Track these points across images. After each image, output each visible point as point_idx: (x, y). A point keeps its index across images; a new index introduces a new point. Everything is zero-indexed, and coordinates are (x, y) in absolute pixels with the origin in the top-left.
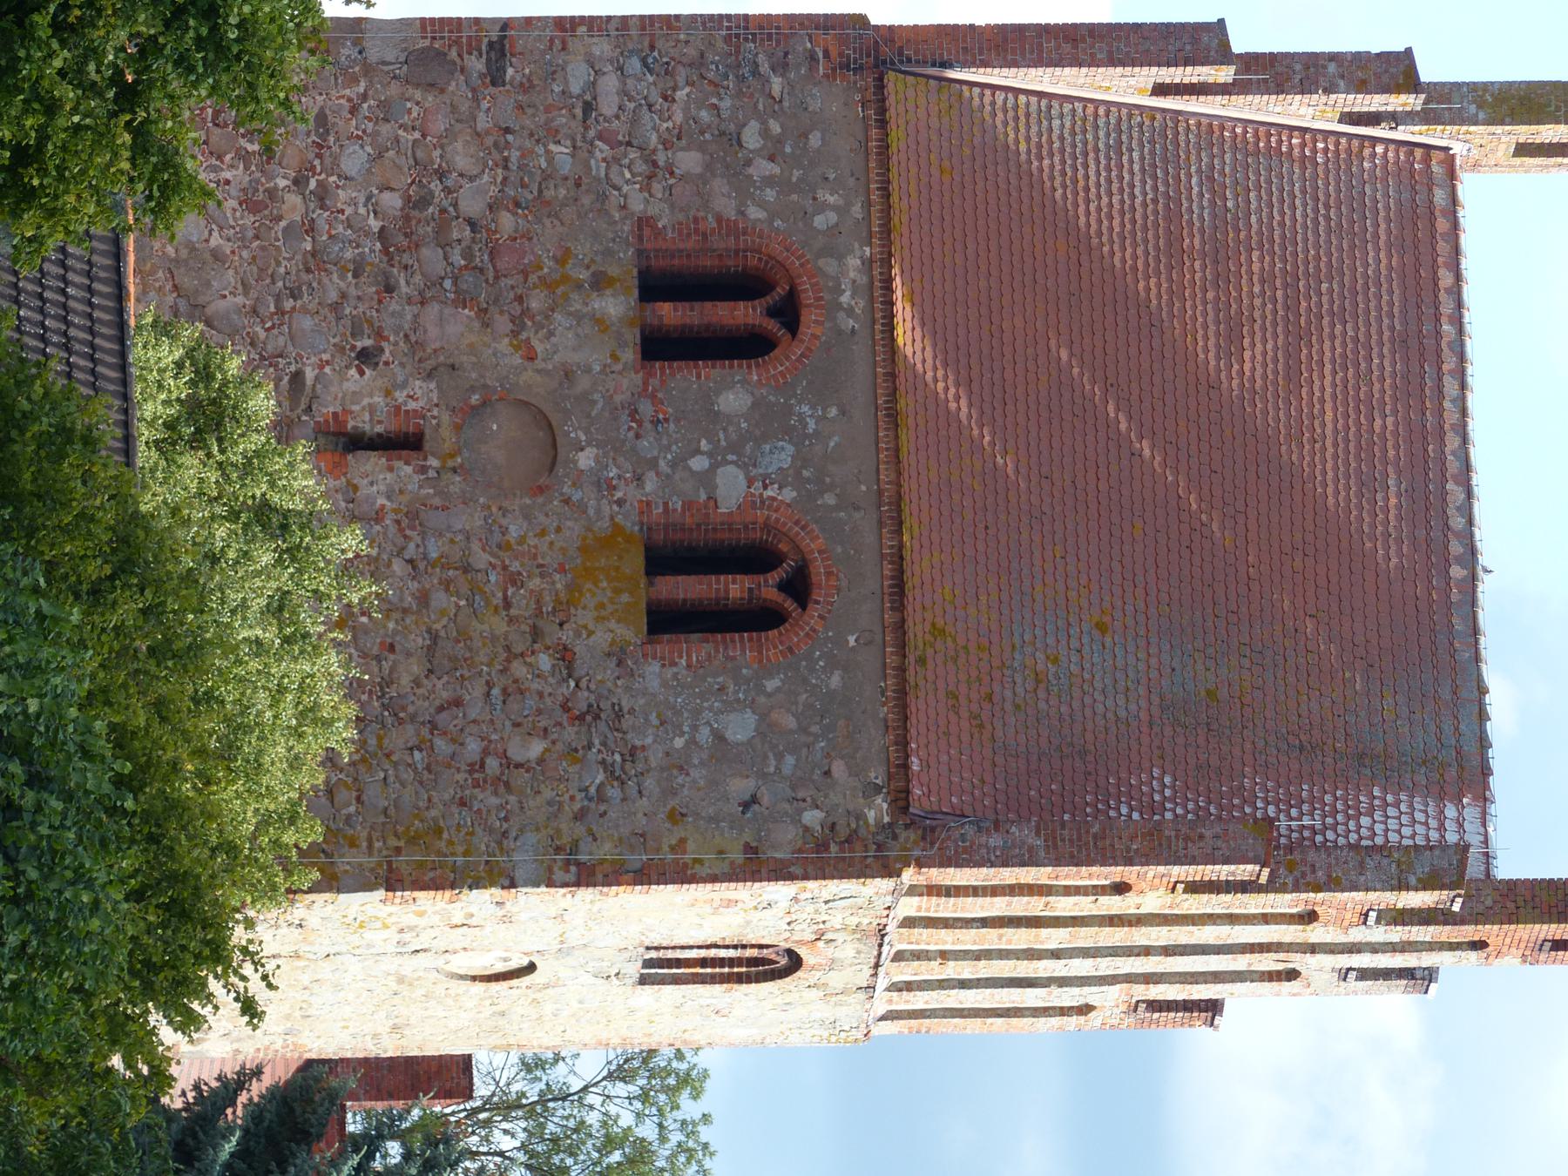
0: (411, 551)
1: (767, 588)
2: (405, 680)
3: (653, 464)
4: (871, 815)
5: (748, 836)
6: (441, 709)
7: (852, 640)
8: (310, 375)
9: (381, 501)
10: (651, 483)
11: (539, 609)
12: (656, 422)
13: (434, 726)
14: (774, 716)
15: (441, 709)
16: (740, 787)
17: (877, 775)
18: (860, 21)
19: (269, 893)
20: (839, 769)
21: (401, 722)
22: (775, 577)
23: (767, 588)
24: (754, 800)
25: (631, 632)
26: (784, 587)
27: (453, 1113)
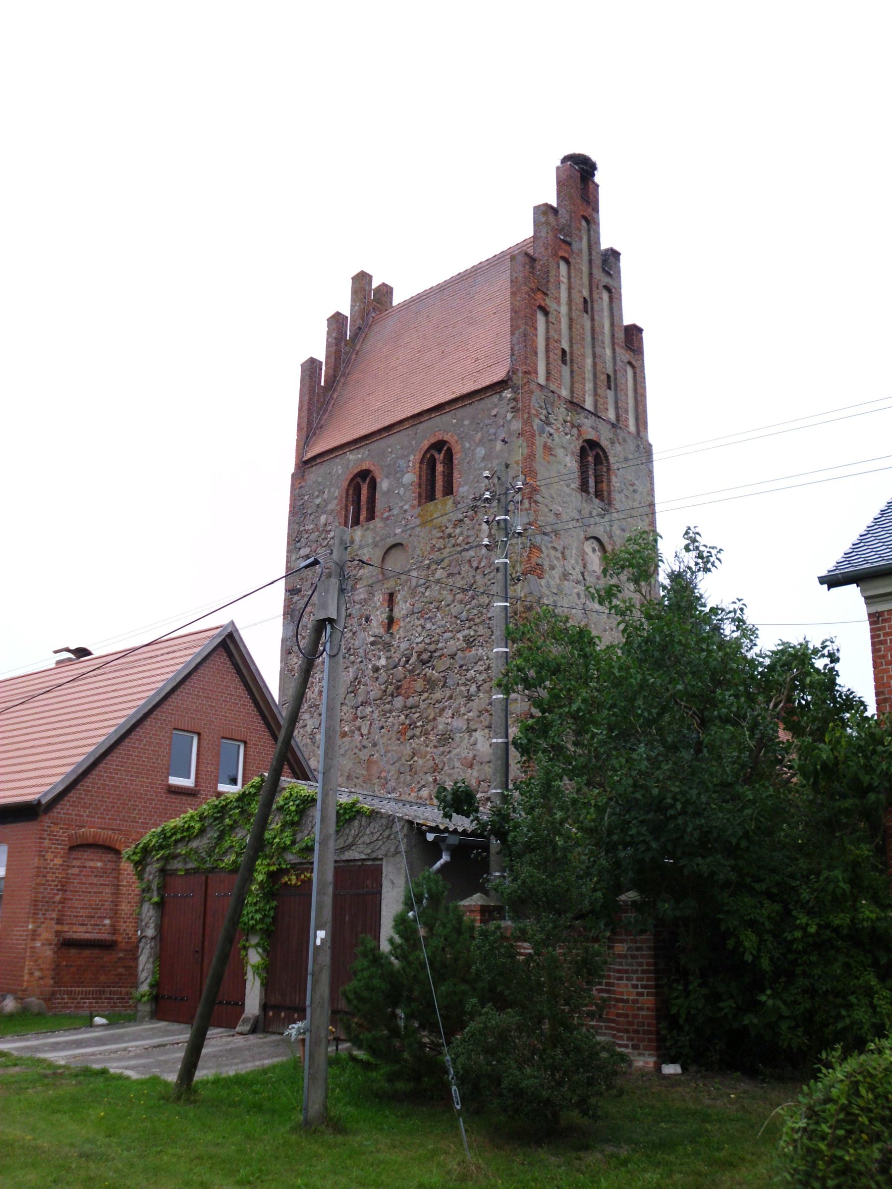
0: (423, 590)
1: (440, 457)
2: (462, 582)
3: (401, 507)
4: (509, 396)
5: (515, 439)
6: (471, 567)
7: (454, 421)
8: (372, 639)
9: (408, 604)
10: (406, 507)
11: (441, 537)
12: (390, 510)
13: (477, 568)
14: (477, 441)
15: (471, 567)
16: (499, 445)
17: (495, 398)
18: (293, 475)
19: (9, 848)
20: (494, 412)
21: (475, 582)
22: (437, 456)
23: (440, 457)
24: (503, 441)
25: (450, 500)
26: (440, 451)
27: (626, 1046)
